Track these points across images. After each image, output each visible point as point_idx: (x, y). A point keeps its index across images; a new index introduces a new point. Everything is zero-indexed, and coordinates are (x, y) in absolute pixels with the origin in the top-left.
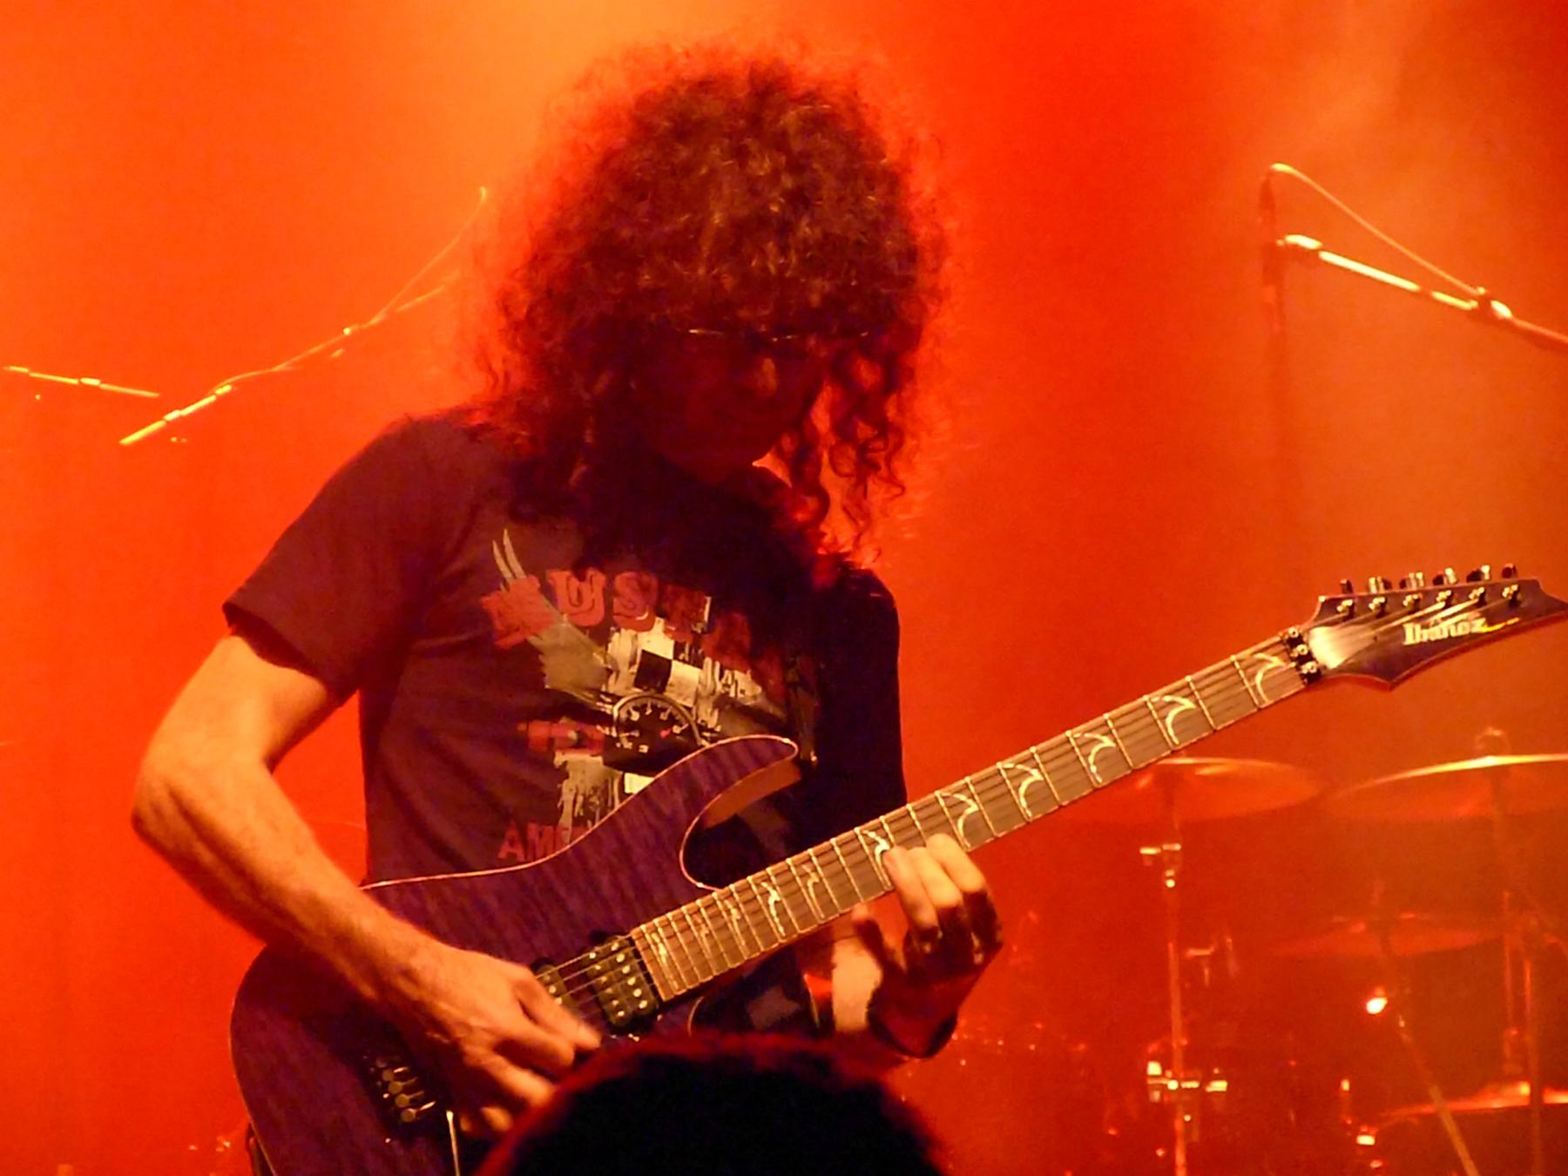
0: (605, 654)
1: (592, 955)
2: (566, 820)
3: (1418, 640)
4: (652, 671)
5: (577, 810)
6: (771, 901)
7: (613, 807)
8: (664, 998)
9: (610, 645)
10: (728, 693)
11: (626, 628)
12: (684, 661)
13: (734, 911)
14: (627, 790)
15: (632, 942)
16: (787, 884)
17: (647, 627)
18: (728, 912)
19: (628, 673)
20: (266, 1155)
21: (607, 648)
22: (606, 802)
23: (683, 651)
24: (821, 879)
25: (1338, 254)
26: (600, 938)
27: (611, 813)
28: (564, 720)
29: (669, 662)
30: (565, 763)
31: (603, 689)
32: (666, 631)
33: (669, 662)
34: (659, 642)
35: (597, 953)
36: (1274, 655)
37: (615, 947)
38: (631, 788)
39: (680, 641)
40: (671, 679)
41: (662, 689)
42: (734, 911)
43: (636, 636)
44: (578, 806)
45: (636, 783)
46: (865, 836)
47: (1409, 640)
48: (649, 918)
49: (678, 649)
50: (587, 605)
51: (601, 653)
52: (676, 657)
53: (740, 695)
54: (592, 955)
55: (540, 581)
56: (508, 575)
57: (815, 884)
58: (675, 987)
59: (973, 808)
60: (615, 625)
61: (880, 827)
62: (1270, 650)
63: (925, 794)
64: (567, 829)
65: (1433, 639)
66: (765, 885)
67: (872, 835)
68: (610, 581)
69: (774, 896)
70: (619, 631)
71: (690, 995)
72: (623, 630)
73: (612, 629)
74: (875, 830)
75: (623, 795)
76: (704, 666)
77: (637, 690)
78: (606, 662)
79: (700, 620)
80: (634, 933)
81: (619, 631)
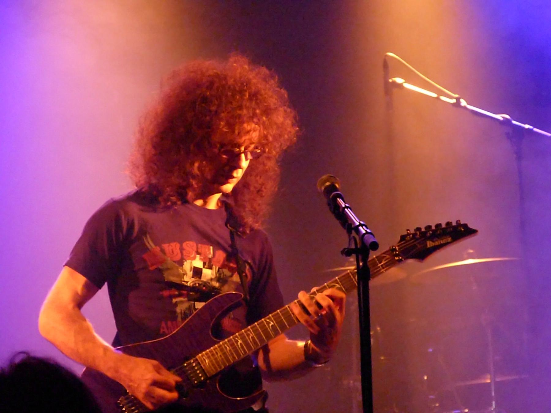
0: (182, 269)
1: (185, 365)
2: (179, 319)
3: (431, 246)
4: (197, 272)
5: (182, 316)
6: (239, 344)
7: (193, 313)
8: (208, 376)
9: (184, 266)
10: (221, 276)
11: (188, 260)
12: (206, 268)
13: (228, 348)
14: (196, 308)
15: (197, 360)
16: (243, 338)
17: (194, 258)
18: (226, 348)
19: (190, 274)
20: (244, 347)
21: (183, 267)
22: (191, 311)
23: (206, 265)
24: (275, 324)
25: (446, 89)
26: (187, 359)
27: (193, 315)
28: (173, 289)
29: (201, 269)
30: (176, 302)
31: (183, 280)
32: (200, 259)
33: (201, 269)
34: (198, 263)
35: (187, 364)
36: (388, 255)
37: (192, 361)
38: (197, 307)
39: (205, 262)
40: (203, 275)
41: (200, 278)
42: (228, 348)
43: (191, 263)
44: (182, 314)
45: (199, 305)
46: (266, 321)
47: (428, 246)
48: (201, 352)
49: (204, 264)
50: (175, 253)
51: (181, 269)
52: (204, 267)
53: (224, 276)
54: (185, 365)
55: (160, 248)
56: (150, 247)
57: (252, 337)
58: (213, 372)
59: (272, 323)
60: (185, 259)
61: (269, 318)
62: (387, 253)
63: (332, 278)
64: (180, 322)
65: (436, 245)
66: (236, 338)
67: (268, 320)
68: (181, 245)
69: (240, 341)
70: (186, 261)
71: (216, 375)
72: (187, 261)
73: (184, 261)
74: (268, 319)
75: (196, 309)
76: (213, 268)
77: (193, 279)
78: (183, 271)
79: (210, 253)
80: (197, 357)
81: (186, 261)
